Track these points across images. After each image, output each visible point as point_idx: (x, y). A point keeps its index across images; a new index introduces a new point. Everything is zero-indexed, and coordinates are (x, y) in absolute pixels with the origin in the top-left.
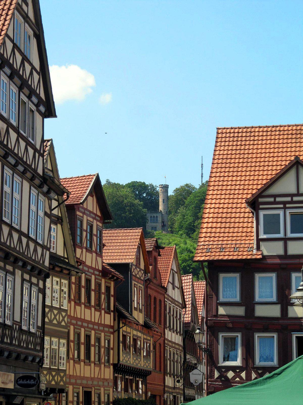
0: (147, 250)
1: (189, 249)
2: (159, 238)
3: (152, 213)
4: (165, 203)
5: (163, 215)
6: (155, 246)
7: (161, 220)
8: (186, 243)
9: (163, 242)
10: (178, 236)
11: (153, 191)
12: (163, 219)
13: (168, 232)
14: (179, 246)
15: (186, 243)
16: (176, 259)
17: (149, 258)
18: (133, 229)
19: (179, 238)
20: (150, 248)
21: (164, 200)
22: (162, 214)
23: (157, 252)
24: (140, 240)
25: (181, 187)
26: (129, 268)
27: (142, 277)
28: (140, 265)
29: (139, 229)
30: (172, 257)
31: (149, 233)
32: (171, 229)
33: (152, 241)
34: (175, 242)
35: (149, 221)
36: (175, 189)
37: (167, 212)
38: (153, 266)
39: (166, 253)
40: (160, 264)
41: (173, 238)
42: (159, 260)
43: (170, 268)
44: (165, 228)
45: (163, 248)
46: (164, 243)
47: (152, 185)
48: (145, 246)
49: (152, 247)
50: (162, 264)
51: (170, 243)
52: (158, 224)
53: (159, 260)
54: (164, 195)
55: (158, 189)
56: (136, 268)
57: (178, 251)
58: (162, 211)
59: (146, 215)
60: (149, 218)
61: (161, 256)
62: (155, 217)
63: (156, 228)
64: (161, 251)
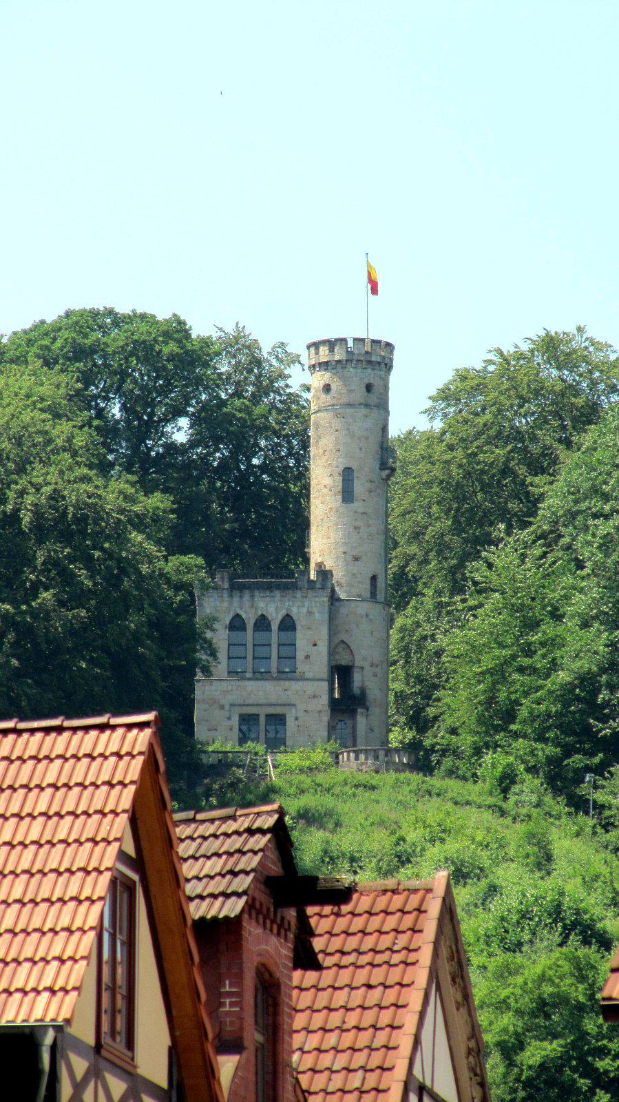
0: (197, 911)
1: (578, 913)
2: (309, 818)
3: (250, 587)
4: (357, 505)
5: (344, 611)
6: (268, 882)
7: (323, 648)
8: (544, 861)
9: (345, 847)
10: (473, 797)
11: (255, 399)
12: (337, 644)
13: (383, 754)
14: (483, 884)
15: (549, 858)
16: (452, 994)
17: (216, 998)
18: (75, 730)
19: (487, 816)
20: (226, 896)
21: (347, 475)
22: (334, 598)
23: (281, 928)
24: (134, 821)
25: (508, 364)
26: (40, 1072)
27: (79, 1074)
28: (130, 1044)
29: (130, 727)
30: (421, 976)
31: (223, 765)
32: (410, 735)
33: (237, 833)
34: (452, 847)
35: (222, 655)
36: (443, 377)
37: (374, 578)
38: (249, 1054)
39: (369, 942)
40: (313, 1041)
41: (432, 811)
42: (305, 1000)
43: (400, 1073)
44: (361, 721)
45: (340, 896)
46: (353, 860)
47: (240, 345)
48: (177, 881)
49: (243, 883)
50: (331, 1040)
51: (403, 860)
52: (296, 686)
53: (305, 1000)
54: (350, 433)
55: (298, 379)
56: (94, 1073)
57: (472, 926)
58: (338, 575)
59: (188, 608)
60: (220, 637)
61: (318, 967)
62: (275, 627)
63: (278, 720)
64: (321, 918)
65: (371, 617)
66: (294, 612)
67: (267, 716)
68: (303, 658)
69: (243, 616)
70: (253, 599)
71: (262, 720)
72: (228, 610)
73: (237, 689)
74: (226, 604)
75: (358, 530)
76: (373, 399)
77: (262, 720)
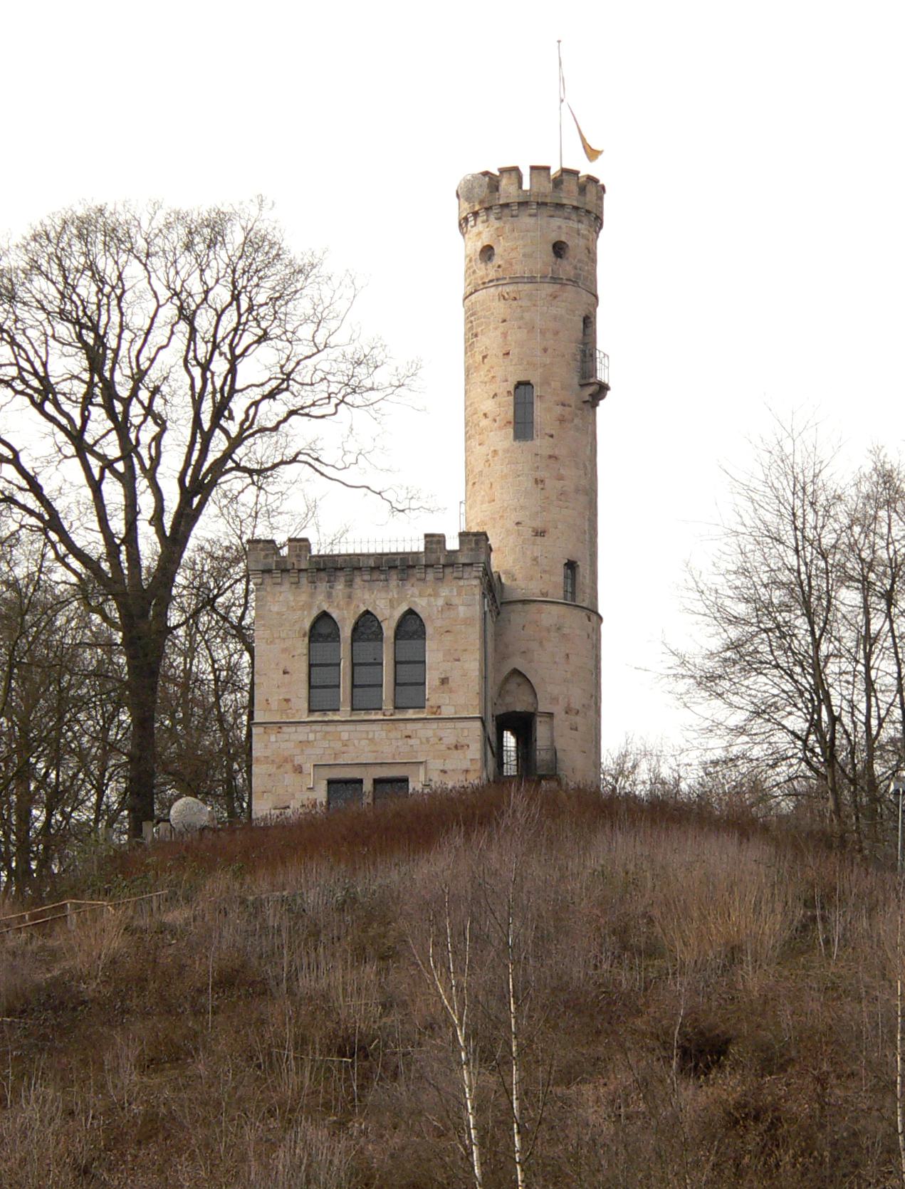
4: (540, 444)
65: (566, 631)
66: (422, 605)
67: (377, 782)
68: (437, 683)
69: (334, 616)
70: (350, 586)
71: (368, 786)
72: (309, 606)
73: (324, 738)
74: (304, 598)
75: (540, 486)
76: (566, 268)
77: (368, 786)
